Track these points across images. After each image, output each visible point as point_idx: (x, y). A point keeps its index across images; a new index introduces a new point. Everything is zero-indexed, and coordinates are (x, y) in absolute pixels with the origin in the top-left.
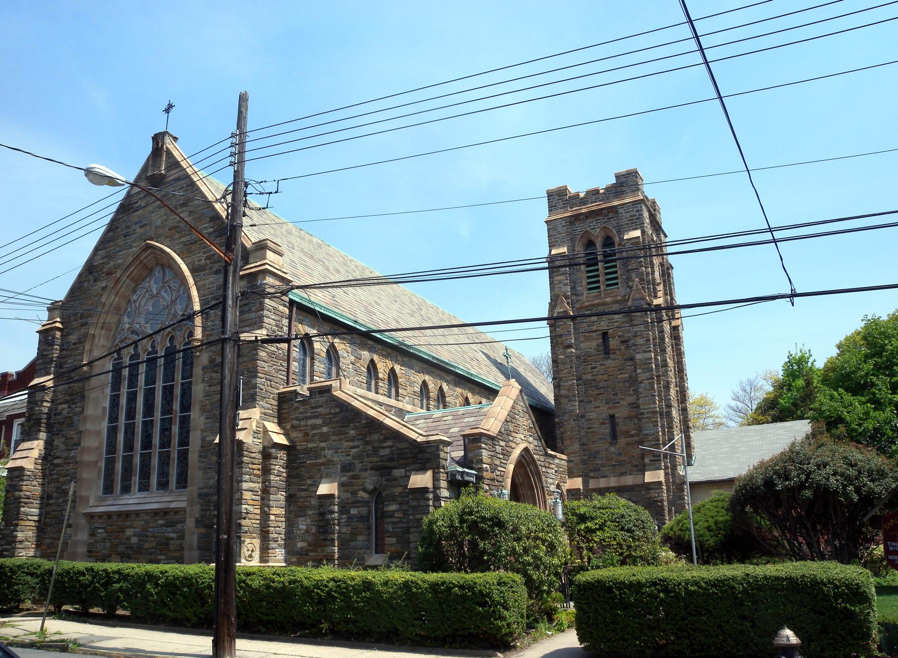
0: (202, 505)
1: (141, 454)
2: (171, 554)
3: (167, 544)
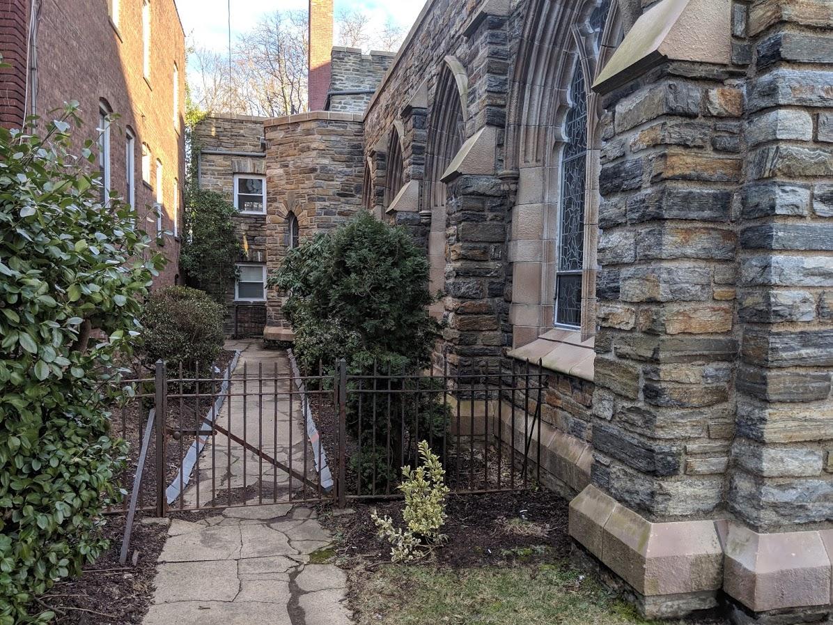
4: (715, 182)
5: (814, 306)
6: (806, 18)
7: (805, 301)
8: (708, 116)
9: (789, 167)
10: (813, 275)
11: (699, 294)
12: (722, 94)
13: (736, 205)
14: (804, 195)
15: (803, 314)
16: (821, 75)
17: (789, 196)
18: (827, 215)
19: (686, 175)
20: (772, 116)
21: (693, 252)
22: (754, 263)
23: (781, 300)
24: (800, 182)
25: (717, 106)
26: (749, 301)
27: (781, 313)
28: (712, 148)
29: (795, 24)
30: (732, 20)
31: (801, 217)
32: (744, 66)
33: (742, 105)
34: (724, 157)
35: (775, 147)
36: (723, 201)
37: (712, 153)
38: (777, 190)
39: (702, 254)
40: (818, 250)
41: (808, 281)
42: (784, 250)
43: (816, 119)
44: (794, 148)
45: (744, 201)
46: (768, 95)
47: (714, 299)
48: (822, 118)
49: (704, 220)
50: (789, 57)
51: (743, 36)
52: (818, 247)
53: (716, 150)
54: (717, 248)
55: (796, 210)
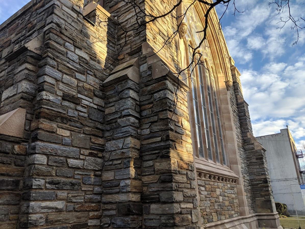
4: (14, 176)
5: (44, 220)
6: (46, 129)
7: (41, 218)
8: (13, 154)
9: (38, 172)
10: (45, 208)
11: (3, 218)
12: (19, 147)
13: (21, 184)
14: (43, 182)
15: (40, 223)
16: (50, 145)
17: (38, 182)
18: (50, 188)
19: (2, 174)
20: (34, 155)
21: (2, 202)
22: (25, 205)
23: (33, 218)
24: (41, 177)
25: (17, 151)
26: (22, 220)
27: (32, 223)
28: (14, 165)
29: (43, 130)
30: (25, 125)
31: (41, 189)
32: (28, 139)
33: (26, 151)
34: (18, 168)
35: (34, 166)
36: (16, 183)
37: (14, 166)
38: (34, 180)
39: (6, 202)
40: (47, 200)
41: (43, 211)
42: (35, 200)
43: (48, 158)
44: (40, 167)
45: (24, 183)
46: (33, 149)
47: (9, 220)
48: (50, 158)
49: (8, 190)
50: (40, 139)
51: (28, 130)
52: (47, 199)
53: (15, 165)
54: (13, 200)
55: (40, 187)
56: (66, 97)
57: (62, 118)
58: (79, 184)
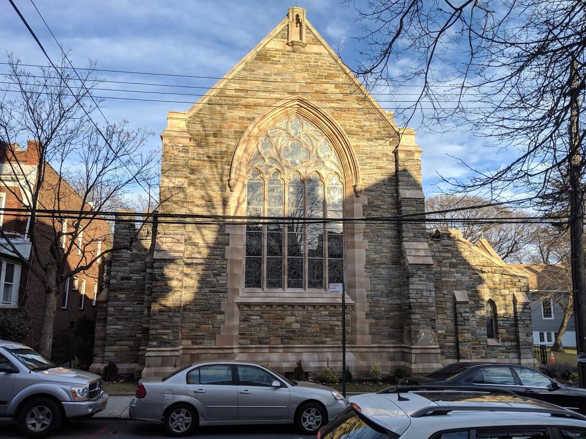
0: (370, 303)
1: (288, 258)
2: (336, 337)
3: (333, 329)
56: (123, 278)
57: (120, 289)
58: (131, 319)
